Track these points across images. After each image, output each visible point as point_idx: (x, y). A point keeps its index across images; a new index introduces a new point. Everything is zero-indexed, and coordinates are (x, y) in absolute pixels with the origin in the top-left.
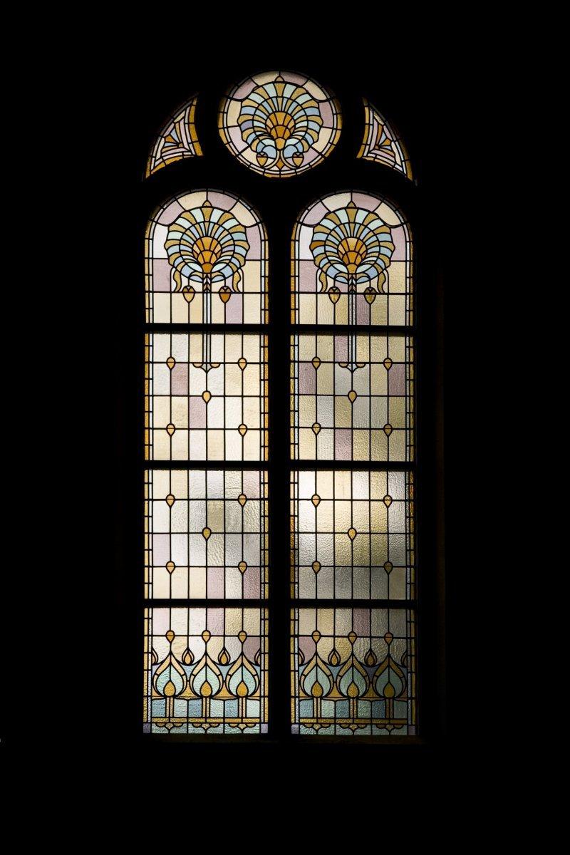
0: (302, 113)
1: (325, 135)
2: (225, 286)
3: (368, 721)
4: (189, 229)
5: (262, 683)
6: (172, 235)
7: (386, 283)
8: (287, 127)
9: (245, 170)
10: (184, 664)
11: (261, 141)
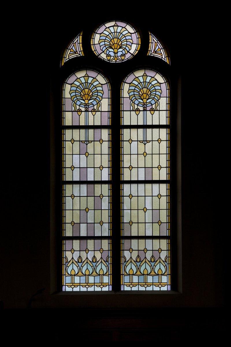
0: (125, 38)
1: (134, 47)
4: (137, 85)
6: (72, 88)
7: (100, 107)
9: (102, 61)
11: (108, 50)
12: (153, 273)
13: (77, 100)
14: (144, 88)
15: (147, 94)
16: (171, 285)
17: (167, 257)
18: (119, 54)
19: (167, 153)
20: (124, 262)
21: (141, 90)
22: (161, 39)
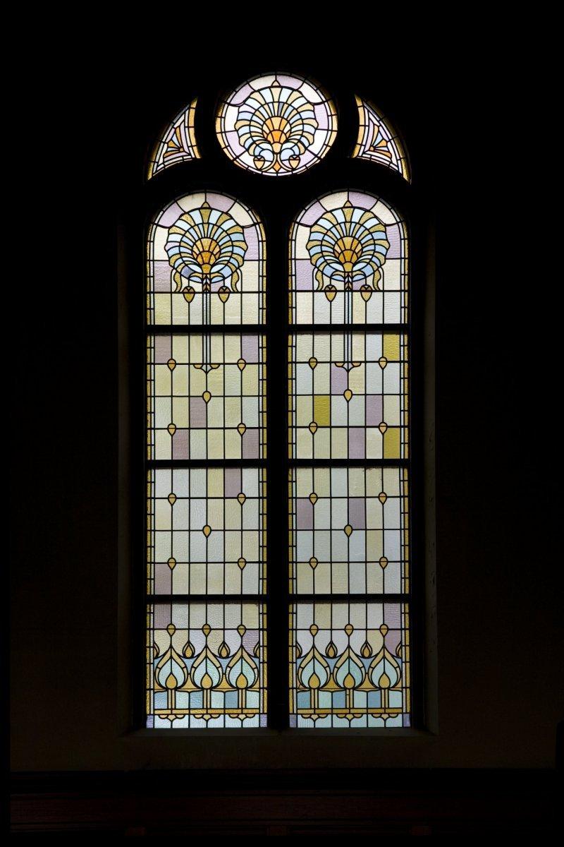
1: (320, 137)
3: (222, 711)
5: (404, 675)
7: (381, 280)
9: (246, 173)
10: (363, 657)
12: (224, 685)
13: (183, 265)
14: (347, 236)
15: (212, 253)
16: (410, 713)
17: (259, 647)
21: (197, 243)
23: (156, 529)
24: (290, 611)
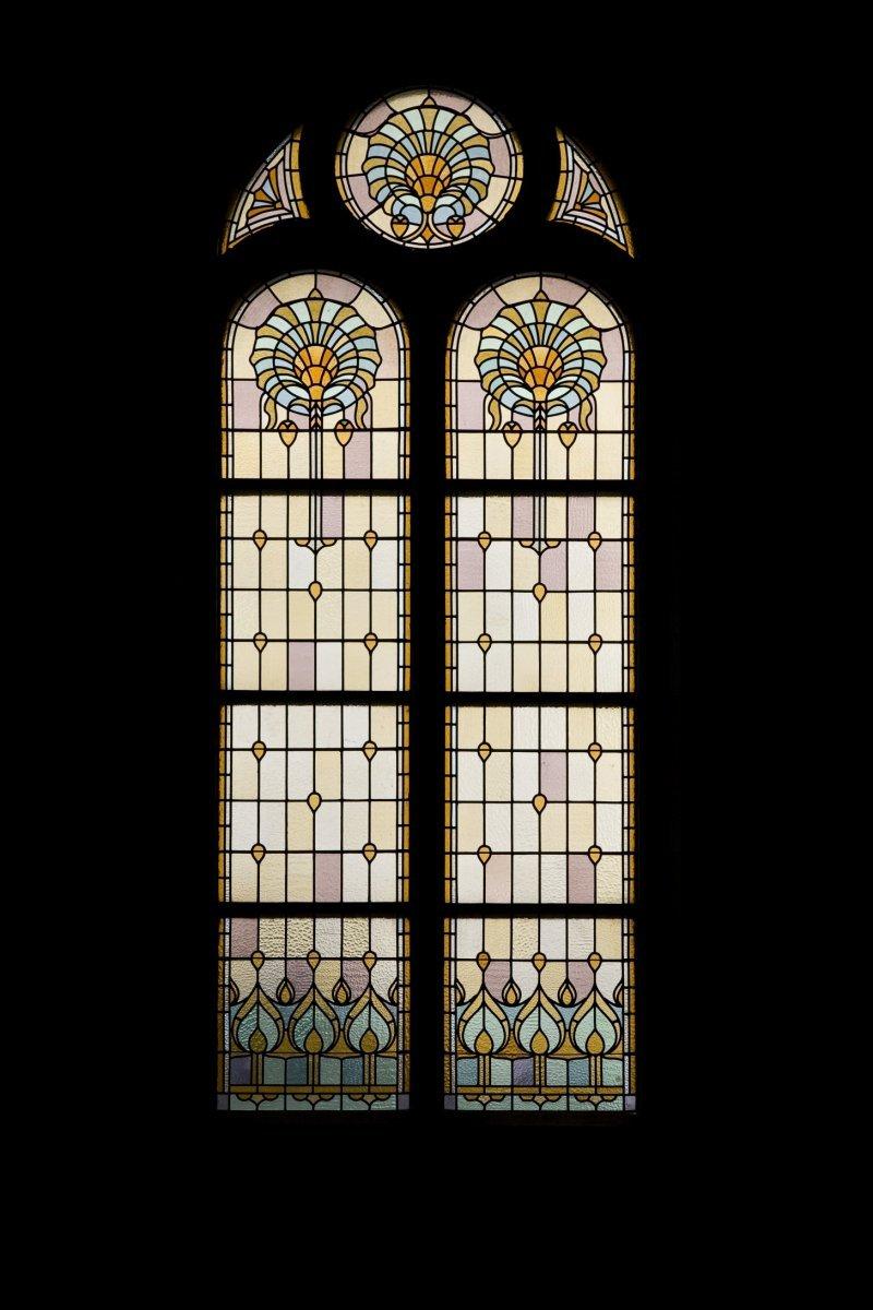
0: (463, 156)
1: (498, 188)
2: (568, 421)
8: (438, 178)
9: (376, 239)
13: (280, 387)
17: (623, 988)
18: (442, 216)
19: (401, 587)
20: (457, 1005)
22: (601, 156)
23: (395, 803)
24: (447, 930)
